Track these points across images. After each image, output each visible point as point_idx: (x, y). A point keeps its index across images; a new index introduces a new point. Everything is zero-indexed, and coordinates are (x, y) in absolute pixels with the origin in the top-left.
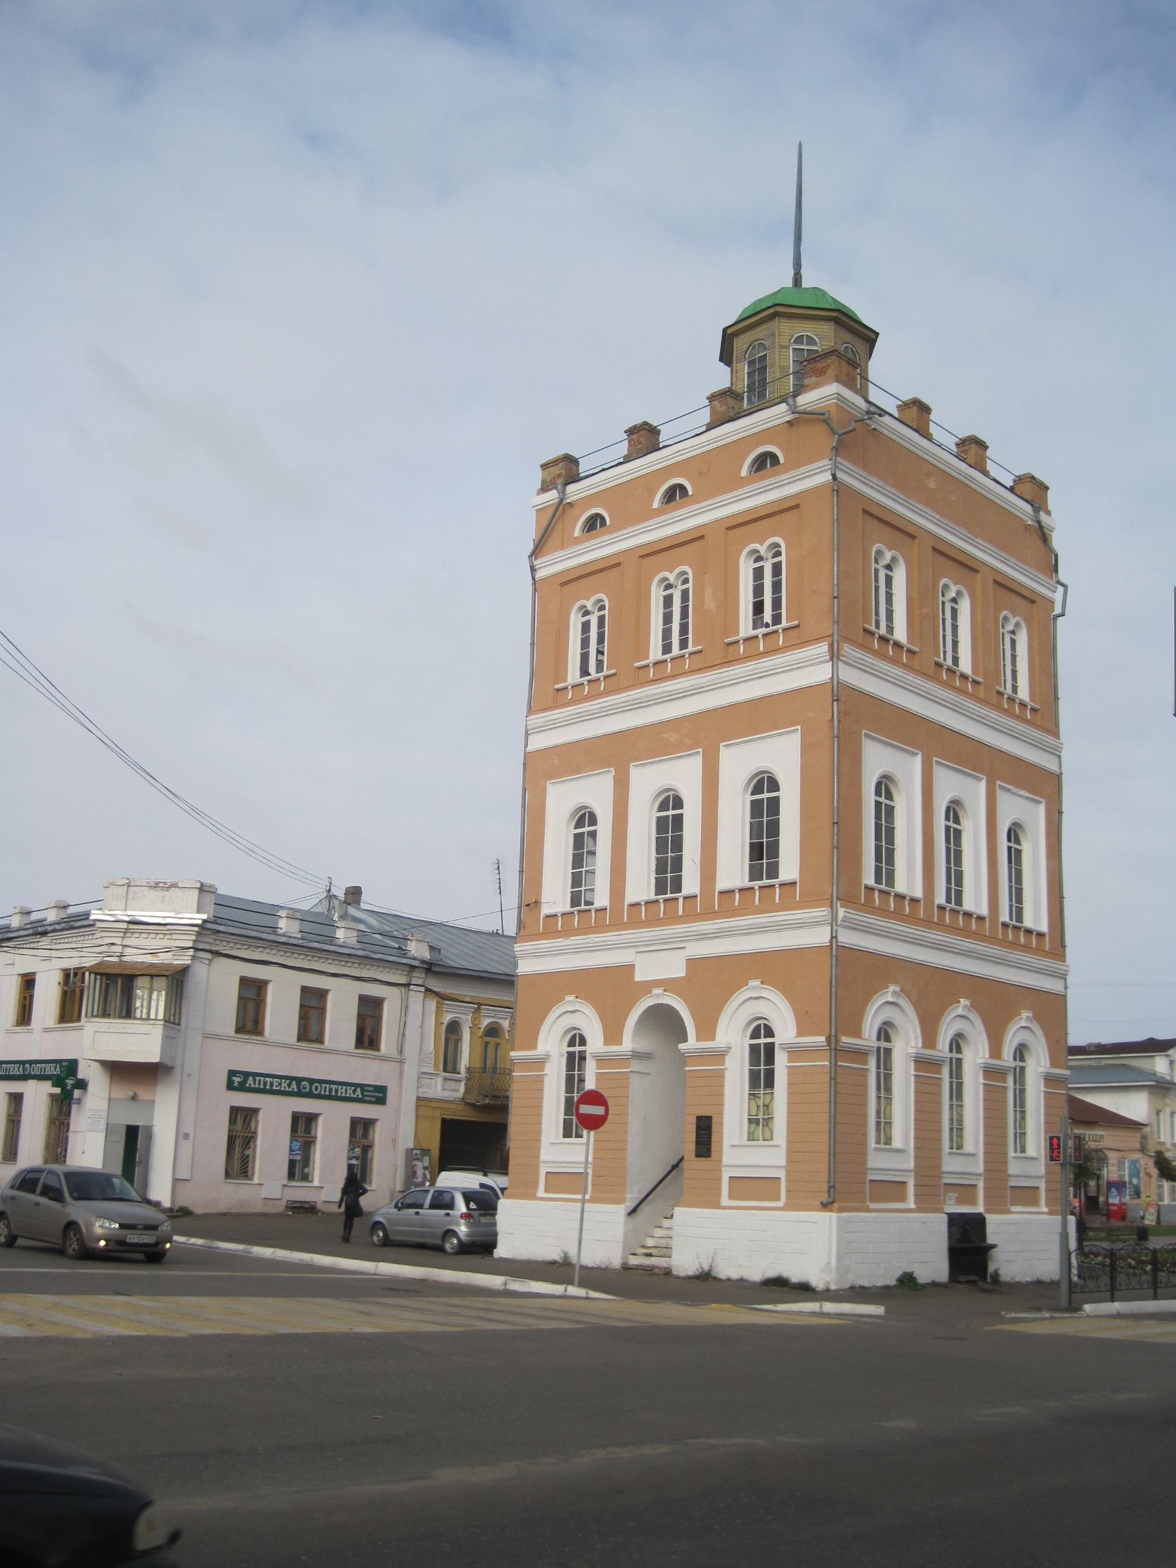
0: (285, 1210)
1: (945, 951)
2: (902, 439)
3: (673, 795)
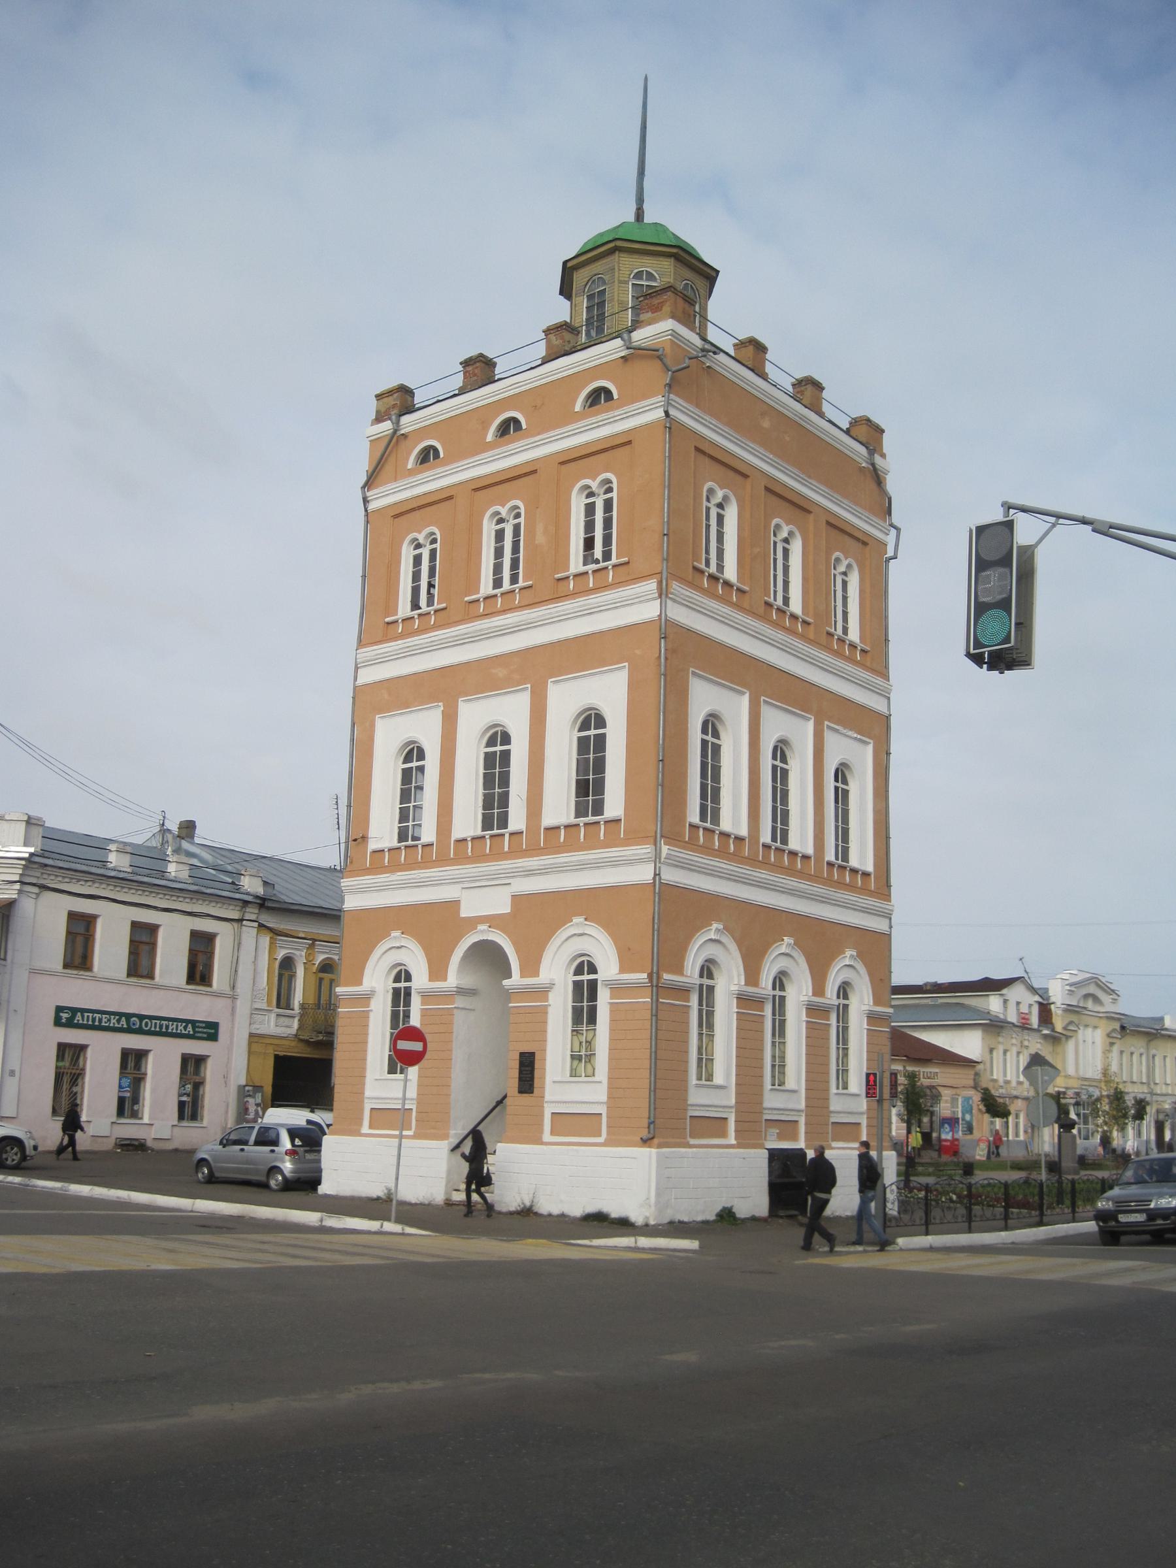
0: (114, 1147)
1: (766, 888)
2: (770, 399)
3: (501, 730)
